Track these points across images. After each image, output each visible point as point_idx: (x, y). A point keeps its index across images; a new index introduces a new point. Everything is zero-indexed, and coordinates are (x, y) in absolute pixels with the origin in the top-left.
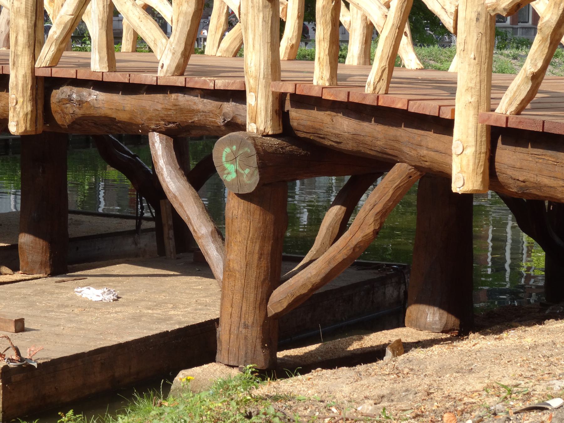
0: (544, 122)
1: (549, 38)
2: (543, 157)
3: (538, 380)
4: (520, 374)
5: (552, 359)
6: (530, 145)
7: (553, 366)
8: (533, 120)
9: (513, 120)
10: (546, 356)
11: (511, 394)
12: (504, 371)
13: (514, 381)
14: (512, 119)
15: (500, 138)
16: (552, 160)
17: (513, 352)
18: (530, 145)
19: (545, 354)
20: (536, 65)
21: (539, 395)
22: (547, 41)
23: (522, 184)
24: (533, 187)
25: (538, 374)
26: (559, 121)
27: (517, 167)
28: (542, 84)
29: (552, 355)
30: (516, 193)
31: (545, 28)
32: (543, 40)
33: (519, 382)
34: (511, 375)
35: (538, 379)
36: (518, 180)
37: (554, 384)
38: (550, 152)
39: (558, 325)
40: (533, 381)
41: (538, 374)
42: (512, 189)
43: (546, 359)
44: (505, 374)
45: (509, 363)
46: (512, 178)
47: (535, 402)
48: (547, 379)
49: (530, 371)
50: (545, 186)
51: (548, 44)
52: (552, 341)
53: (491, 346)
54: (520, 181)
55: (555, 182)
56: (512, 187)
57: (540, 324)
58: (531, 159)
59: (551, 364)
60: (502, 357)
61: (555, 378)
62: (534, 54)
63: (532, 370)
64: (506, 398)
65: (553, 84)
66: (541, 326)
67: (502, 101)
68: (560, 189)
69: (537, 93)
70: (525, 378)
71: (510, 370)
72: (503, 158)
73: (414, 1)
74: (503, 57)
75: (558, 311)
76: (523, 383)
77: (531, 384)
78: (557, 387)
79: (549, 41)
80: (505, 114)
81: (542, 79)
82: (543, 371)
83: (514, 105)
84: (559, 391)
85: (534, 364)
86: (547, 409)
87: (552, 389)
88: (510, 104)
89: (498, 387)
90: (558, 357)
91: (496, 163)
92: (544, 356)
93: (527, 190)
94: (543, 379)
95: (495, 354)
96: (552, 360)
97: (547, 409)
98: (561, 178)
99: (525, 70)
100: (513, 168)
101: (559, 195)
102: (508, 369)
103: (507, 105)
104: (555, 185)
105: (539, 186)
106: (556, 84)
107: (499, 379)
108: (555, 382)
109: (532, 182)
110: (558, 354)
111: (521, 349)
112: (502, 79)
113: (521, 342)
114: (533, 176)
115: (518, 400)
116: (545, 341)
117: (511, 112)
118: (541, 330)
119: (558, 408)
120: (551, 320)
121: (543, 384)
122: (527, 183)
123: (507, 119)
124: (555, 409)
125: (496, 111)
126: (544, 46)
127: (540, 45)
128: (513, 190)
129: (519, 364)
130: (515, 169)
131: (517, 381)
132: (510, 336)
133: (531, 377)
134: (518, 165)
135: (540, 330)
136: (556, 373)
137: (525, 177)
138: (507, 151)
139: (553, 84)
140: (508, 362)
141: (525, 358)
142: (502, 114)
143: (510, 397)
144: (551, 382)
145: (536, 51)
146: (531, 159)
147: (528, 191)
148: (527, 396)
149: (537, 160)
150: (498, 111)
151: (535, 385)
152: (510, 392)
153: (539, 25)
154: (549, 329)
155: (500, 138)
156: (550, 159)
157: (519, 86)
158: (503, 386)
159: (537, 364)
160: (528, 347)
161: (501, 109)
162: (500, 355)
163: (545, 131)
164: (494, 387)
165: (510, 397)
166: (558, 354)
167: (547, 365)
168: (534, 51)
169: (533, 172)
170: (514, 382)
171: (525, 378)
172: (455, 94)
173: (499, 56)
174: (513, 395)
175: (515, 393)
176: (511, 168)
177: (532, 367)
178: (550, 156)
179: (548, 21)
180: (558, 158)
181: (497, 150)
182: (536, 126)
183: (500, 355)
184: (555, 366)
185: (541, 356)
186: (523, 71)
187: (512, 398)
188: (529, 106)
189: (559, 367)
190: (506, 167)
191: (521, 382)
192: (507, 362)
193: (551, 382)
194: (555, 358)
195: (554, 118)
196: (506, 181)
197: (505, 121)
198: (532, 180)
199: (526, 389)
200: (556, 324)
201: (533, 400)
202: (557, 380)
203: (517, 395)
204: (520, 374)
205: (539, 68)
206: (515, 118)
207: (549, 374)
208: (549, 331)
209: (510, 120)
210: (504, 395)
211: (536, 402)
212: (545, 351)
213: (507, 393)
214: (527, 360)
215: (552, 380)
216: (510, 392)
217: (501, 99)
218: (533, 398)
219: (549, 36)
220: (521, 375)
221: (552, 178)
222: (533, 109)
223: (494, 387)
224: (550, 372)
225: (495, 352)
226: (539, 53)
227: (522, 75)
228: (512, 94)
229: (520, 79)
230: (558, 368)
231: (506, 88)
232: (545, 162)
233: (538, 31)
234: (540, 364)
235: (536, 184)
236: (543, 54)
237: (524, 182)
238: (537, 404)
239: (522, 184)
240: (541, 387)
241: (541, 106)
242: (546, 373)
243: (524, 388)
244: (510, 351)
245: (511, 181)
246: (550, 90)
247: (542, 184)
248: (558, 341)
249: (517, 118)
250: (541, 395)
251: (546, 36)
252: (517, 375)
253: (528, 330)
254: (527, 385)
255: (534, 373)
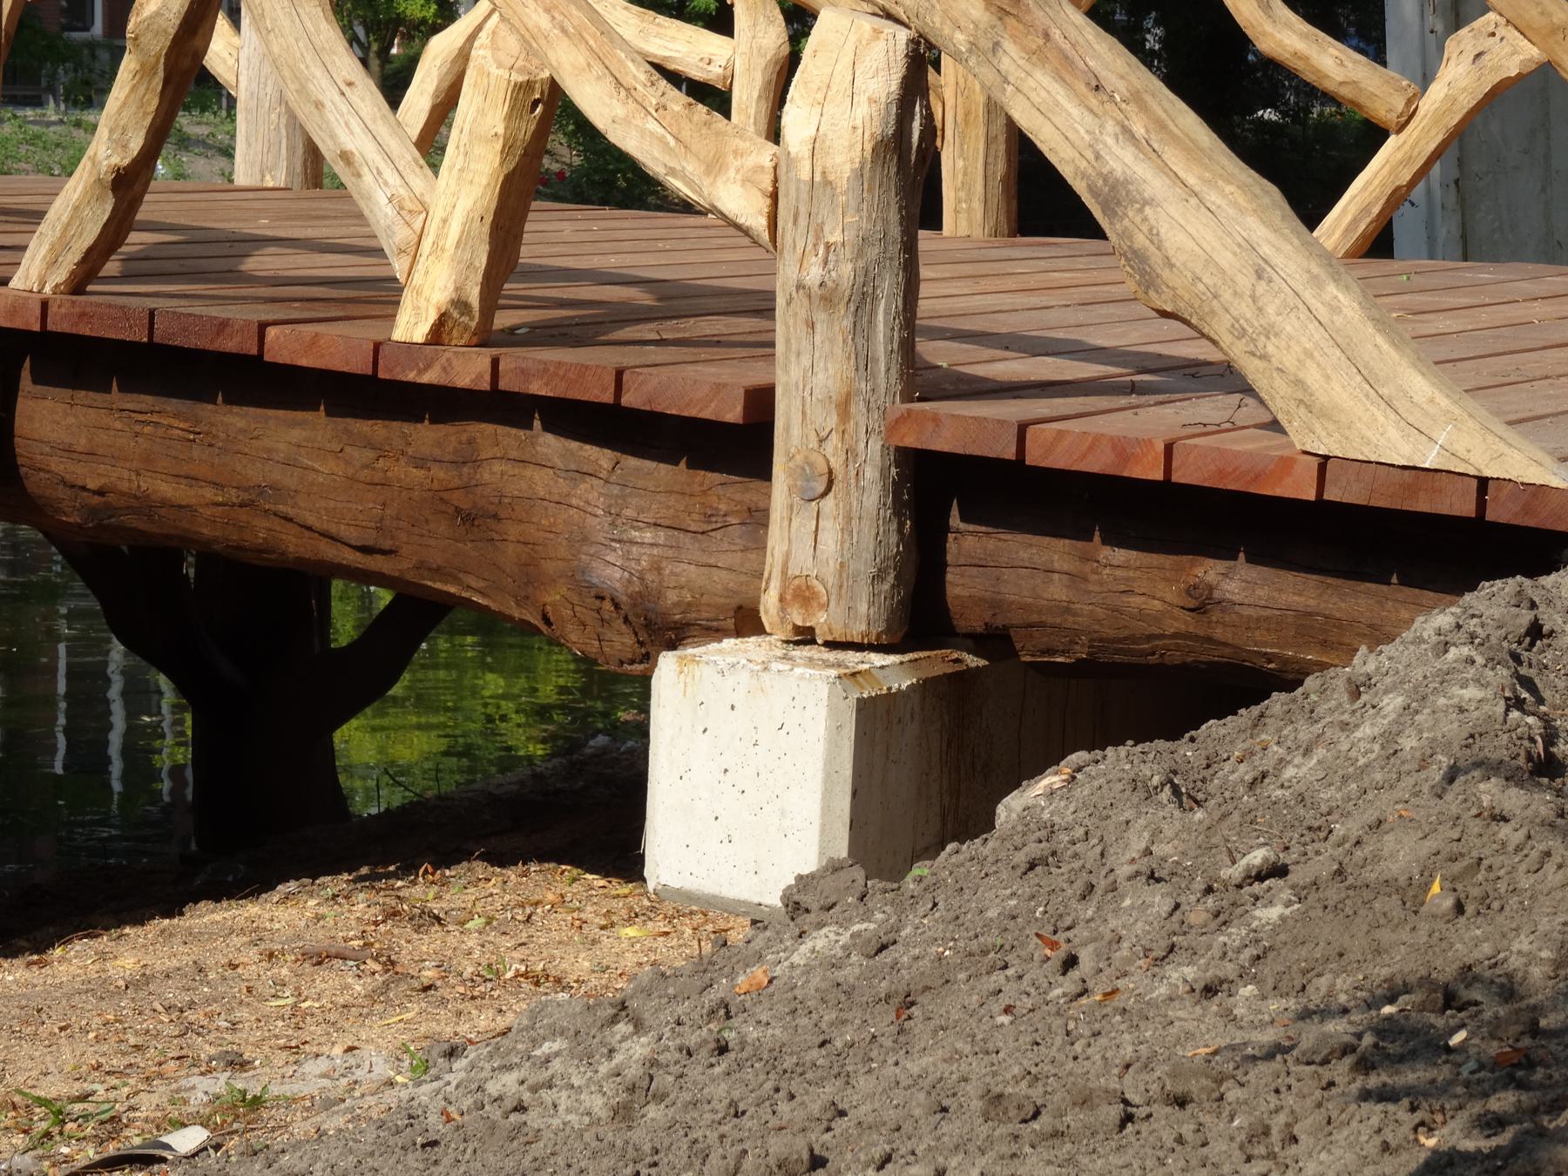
0: (152, 313)
1: (161, 67)
2: (155, 418)
3: (147, 1078)
4: (94, 1062)
5: (191, 1016)
6: (115, 384)
7: (195, 1036)
8: (122, 308)
9: (63, 310)
10: (175, 1006)
11: (63, 1122)
12: (49, 1058)
13: (77, 1085)
14: (59, 307)
15: (27, 363)
16: (181, 426)
17: (76, 1000)
18: (115, 384)
19: (173, 1001)
20: (125, 147)
21: (146, 1120)
22: (155, 73)
23: (96, 500)
24: (128, 508)
25: (145, 1061)
26: (197, 310)
27: (80, 449)
28: (143, 207)
29: (191, 1005)
30: (79, 526)
31: (150, 36)
32: (145, 72)
33: (88, 1087)
34: (67, 1068)
35: (147, 1074)
36: (84, 488)
37: (193, 1088)
38: (174, 404)
39: (217, 917)
40: (132, 1081)
41: (145, 1061)
42: (66, 514)
43: (174, 1017)
44: (49, 1065)
45: (63, 1034)
46: (64, 482)
47: (133, 1140)
48: (173, 1075)
49: (124, 1054)
50: (165, 503)
51: (158, 82)
52: (195, 962)
53: (14, 987)
54: (88, 490)
55: (192, 492)
56: (67, 509)
57: (169, 914)
58: (118, 425)
59: (189, 1028)
60: (44, 1016)
61: (196, 1070)
62: (119, 112)
63: (130, 1050)
64: (48, 1135)
65: (197, 205)
66: (167, 921)
67: (28, 254)
68: (208, 512)
69: (130, 229)
70: (108, 1073)
71: (67, 1055)
72: (37, 425)
73: (191, 4)
74: (82, 131)
75: (230, 878)
76: (100, 1089)
77: (126, 1090)
78: (200, 1095)
79: (161, 74)
80: (39, 292)
81: (144, 191)
82: (163, 1053)
83: (64, 264)
84: (205, 1105)
85: (137, 1033)
86: (163, 1160)
87: (185, 1102)
88: (53, 263)
89: (27, 1106)
90: (210, 1008)
91: (17, 440)
92: (168, 1009)
93: (110, 517)
94: (160, 1075)
95: (22, 1008)
96: (192, 1018)
97: (163, 1160)
98: (210, 479)
99: (93, 160)
100: (66, 454)
101: (205, 531)
102: (58, 1051)
103: (44, 266)
104: (193, 501)
105: (145, 505)
106: (203, 205)
107: (30, 1083)
108: (195, 1080)
109: (122, 494)
110: (208, 1001)
111: (102, 989)
112: (44, 191)
113: (104, 971)
114: (126, 474)
115: (84, 1138)
116: (175, 963)
117: (57, 286)
118: (167, 933)
119: (194, 1155)
120: (202, 904)
121: (161, 1087)
122: (110, 498)
123: (45, 305)
124: (187, 1158)
125: (12, 284)
126: (147, 89)
127: (134, 86)
128: (71, 520)
129: (91, 1035)
130: (75, 456)
131: (85, 1085)
132: (72, 953)
133: (128, 1071)
134: (82, 443)
135: (163, 931)
136: (202, 1056)
137: (103, 481)
138: (48, 403)
139: (197, 205)
140: (61, 1029)
141: (111, 1017)
142: (31, 291)
143: (61, 1133)
144: (183, 1082)
145: (124, 104)
146: (118, 425)
147: (113, 520)
148: (108, 1126)
149: (138, 428)
150: (16, 283)
151: (136, 1093)
152: (60, 1118)
153: (130, 26)
154: (190, 927)
155: (27, 363)
156: (176, 423)
157: (76, 208)
158: (41, 1102)
159: (148, 1031)
160: (121, 983)
161: (27, 278)
162: (39, 1011)
163: (157, 339)
164: (15, 1107)
165: (61, 1133)
166: (208, 1001)
167: (176, 1033)
168: (119, 103)
169: (128, 465)
170: (77, 1088)
171: (108, 1073)
172: (398, 303)
173: (72, 129)
174: (70, 1126)
175: (76, 1120)
176: (63, 454)
177: (132, 1041)
178: (176, 416)
179: (157, 14)
180: (198, 422)
181: (20, 399)
182: (130, 326)
183: (39, 1011)
184: (197, 1034)
185: (160, 1008)
186: (89, 164)
187: (66, 1134)
188: (112, 267)
189: (211, 1037)
190: (47, 449)
191: (96, 1086)
192: (57, 1031)
193: (183, 1082)
194: (202, 1013)
195: (183, 302)
196: (48, 493)
197: (38, 312)
198: (124, 486)
199: (106, 1106)
200: (212, 912)
201: (126, 1138)
202: (202, 1074)
203: (79, 1126)
204: (94, 1062)
205: (136, 153)
206: (68, 305)
207: (179, 1058)
208: (190, 934)
209: (53, 310)
210: (44, 1125)
211: (137, 1141)
212: (174, 995)
213: (50, 1122)
214: (116, 1021)
215: (188, 1076)
216: (60, 1118)
217: (24, 248)
218: (127, 1132)
219: (162, 60)
220: (99, 1066)
221: (184, 481)
222: (125, 277)
223: (15, 1107)
224: (184, 1052)
225: (24, 1002)
226: (134, 108)
227: (86, 175)
228: (58, 234)
229: (80, 188)
230: (206, 1042)
231: (37, 216)
232: (161, 431)
233: (129, 45)
234: (154, 1032)
235: (135, 497)
236: (145, 114)
237: (100, 492)
238: (139, 1147)
239: (96, 500)
240: (155, 1099)
241: (143, 269)
242: (171, 1055)
243: (103, 1102)
244: (69, 997)
245: (62, 493)
246: (183, 221)
247: (153, 497)
248: (211, 962)
249: (73, 302)
250: (153, 1122)
251: (152, 60)
252: (84, 1067)
253: (128, 935)
254: (112, 1095)
255: (137, 1059)
